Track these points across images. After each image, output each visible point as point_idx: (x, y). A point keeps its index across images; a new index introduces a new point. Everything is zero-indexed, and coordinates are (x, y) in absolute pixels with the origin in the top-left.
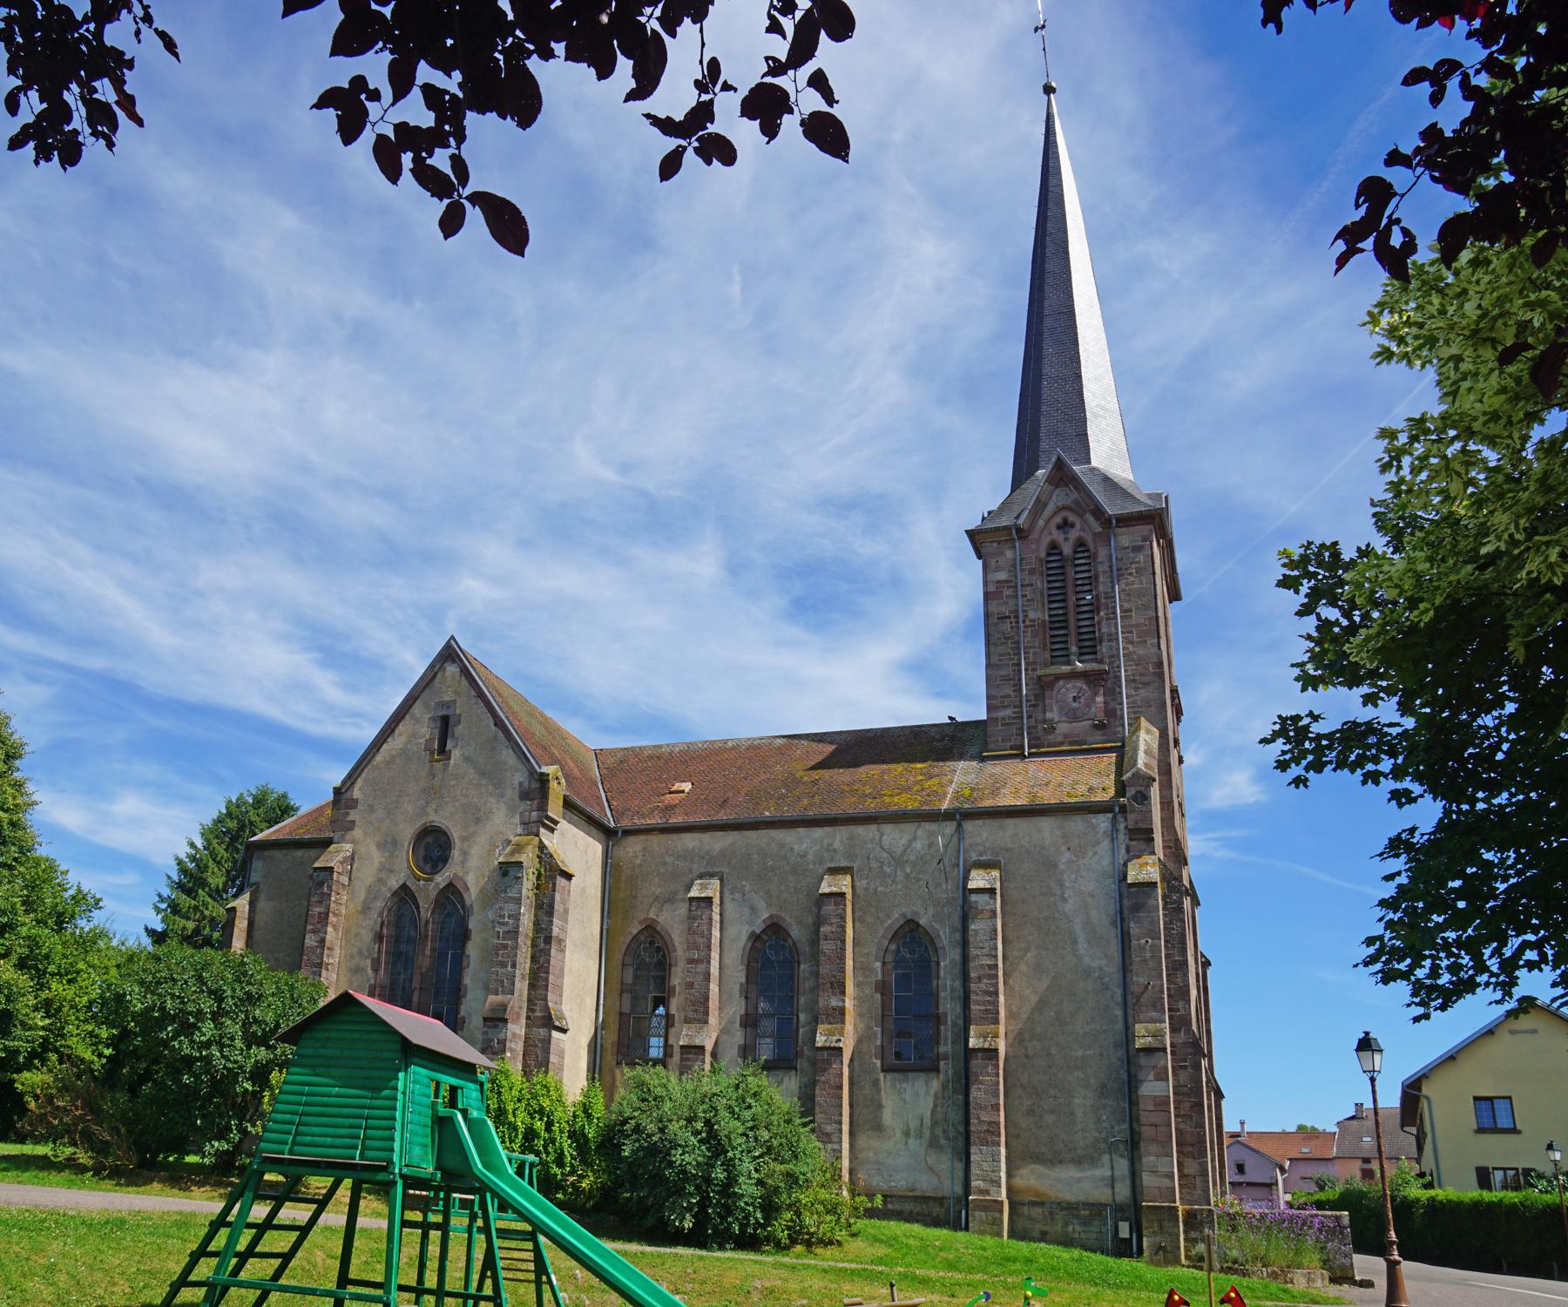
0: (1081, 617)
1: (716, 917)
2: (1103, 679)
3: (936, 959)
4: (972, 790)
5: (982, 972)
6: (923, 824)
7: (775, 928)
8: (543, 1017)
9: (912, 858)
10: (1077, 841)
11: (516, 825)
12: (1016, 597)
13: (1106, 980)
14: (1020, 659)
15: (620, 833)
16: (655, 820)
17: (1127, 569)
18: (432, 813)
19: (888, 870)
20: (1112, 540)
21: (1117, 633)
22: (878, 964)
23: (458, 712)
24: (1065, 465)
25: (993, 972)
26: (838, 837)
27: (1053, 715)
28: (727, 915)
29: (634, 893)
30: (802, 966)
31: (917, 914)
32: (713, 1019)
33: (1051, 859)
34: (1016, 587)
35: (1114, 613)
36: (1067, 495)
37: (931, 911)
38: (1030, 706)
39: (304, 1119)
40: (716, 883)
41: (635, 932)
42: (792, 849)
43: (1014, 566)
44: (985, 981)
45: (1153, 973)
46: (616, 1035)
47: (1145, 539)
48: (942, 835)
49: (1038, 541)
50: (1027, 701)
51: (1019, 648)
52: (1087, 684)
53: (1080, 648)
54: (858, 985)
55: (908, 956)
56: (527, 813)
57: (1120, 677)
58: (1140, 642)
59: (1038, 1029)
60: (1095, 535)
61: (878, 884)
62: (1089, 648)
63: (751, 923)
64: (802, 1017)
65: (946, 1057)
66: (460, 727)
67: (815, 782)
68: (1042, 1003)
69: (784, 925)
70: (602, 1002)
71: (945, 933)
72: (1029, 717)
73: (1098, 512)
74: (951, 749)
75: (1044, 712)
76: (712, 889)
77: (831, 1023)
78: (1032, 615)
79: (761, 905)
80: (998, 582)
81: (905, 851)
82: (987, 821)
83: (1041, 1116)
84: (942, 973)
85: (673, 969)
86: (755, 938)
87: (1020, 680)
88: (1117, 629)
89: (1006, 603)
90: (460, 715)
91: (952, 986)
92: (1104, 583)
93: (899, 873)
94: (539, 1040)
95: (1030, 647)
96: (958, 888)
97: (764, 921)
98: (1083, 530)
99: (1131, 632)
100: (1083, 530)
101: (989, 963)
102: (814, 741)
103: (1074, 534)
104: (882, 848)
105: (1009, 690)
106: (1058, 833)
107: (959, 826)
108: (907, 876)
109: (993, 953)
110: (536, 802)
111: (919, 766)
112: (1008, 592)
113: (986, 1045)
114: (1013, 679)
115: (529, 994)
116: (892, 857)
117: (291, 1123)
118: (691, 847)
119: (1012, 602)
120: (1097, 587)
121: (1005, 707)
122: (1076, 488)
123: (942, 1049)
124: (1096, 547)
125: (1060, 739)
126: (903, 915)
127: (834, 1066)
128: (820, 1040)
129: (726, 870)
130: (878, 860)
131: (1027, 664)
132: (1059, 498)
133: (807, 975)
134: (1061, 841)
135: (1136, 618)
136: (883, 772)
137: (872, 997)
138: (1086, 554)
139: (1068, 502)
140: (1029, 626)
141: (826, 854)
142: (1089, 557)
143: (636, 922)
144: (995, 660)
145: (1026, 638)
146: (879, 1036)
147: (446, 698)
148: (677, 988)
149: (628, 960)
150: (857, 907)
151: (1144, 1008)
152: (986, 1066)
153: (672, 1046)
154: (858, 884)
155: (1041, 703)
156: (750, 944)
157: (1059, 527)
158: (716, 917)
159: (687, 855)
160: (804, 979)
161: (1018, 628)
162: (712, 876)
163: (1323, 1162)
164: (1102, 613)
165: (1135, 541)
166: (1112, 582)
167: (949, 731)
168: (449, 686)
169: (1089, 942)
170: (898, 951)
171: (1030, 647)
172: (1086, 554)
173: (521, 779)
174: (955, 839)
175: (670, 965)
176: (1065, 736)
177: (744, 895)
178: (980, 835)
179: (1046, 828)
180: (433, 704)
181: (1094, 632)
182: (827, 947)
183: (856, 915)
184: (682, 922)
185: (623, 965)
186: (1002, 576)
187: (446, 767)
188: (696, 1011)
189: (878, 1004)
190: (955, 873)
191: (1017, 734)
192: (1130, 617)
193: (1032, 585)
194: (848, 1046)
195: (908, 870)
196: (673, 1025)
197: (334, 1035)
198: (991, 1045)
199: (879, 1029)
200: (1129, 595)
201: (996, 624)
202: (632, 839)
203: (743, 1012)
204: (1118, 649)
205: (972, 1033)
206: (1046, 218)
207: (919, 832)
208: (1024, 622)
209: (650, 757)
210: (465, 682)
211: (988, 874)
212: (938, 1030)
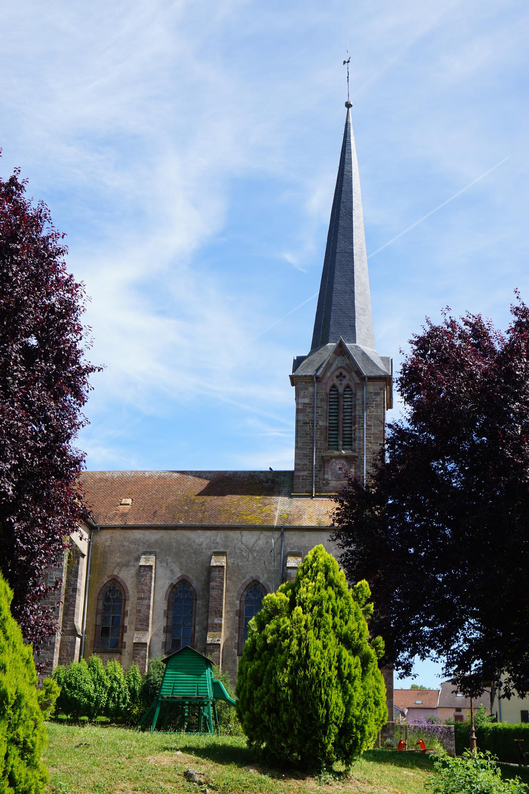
0: (345, 425)
1: (153, 575)
2: (355, 460)
4: (288, 515)
6: (263, 532)
7: (184, 582)
8: (72, 630)
9: (257, 549)
12: (314, 412)
14: (313, 446)
16: (118, 522)
17: (371, 404)
19: (245, 554)
20: (365, 388)
21: (363, 437)
22: (238, 602)
26: (219, 536)
27: (328, 476)
28: (158, 574)
29: (105, 561)
30: (198, 602)
31: (259, 577)
32: (150, 629)
34: (314, 407)
35: (363, 426)
36: (343, 360)
37: (266, 576)
38: (317, 471)
39: (199, 685)
40: (153, 558)
41: (105, 582)
42: (194, 541)
43: (313, 396)
46: (93, 637)
47: (381, 389)
48: (273, 539)
49: (326, 384)
50: (316, 468)
51: (313, 440)
52: (347, 462)
53: (343, 441)
54: (227, 612)
55: (253, 598)
57: (363, 460)
58: (374, 443)
60: (356, 384)
61: (239, 561)
62: (349, 442)
63: (171, 579)
64: (197, 628)
67: (203, 504)
70: (85, 619)
71: (272, 587)
72: (316, 476)
73: (359, 372)
74: (273, 488)
75: (324, 475)
76: (151, 561)
78: (321, 423)
80: (304, 404)
81: (254, 545)
82: (296, 532)
85: (127, 602)
86: (173, 587)
87: (313, 457)
88: (364, 435)
89: (307, 415)
92: (359, 410)
93: (250, 556)
94: (69, 642)
96: (280, 565)
97: (178, 578)
98: (350, 380)
99: (370, 437)
100: (350, 380)
102: (196, 476)
103: (345, 382)
104: (242, 543)
107: (282, 534)
108: (254, 558)
111: (258, 497)
114: (309, 456)
115: (63, 618)
117: (171, 686)
119: (311, 415)
120: (355, 411)
121: (304, 470)
122: (348, 358)
124: (356, 391)
125: (331, 489)
126: (252, 577)
128: (209, 640)
129: (158, 550)
131: (316, 449)
132: (338, 362)
135: (373, 430)
136: (239, 500)
138: (350, 393)
139: (343, 365)
141: (212, 545)
142: (352, 394)
143: (106, 577)
144: (300, 445)
145: (317, 435)
146: (237, 638)
148: (129, 612)
149: (101, 597)
150: (228, 572)
153: (125, 643)
154: (229, 561)
155: (322, 470)
156: (170, 590)
157: (337, 377)
158: (153, 575)
159: (136, 542)
161: (313, 429)
162: (150, 553)
163: (430, 710)
164: (357, 426)
165: (376, 390)
166: (363, 410)
167: (270, 476)
170: (247, 595)
171: (319, 440)
172: (350, 393)
174: (280, 540)
175: (125, 600)
176: (334, 488)
177: (167, 564)
178: (292, 539)
181: (352, 434)
182: (214, 593)
183: (228, 576)
184: (132, 577)
185: (98, 599)
186: (306, 401)
188: (142, 625)
189: (237, 622)
190: (279, 558)
191: (309, 485)
192: (371, 429)
193: (322, 407)
194: (222, 642)
195: (255, 555)
196: (126, 632)
197: (181, 659)
199: (237, 635)
200: (371, 418)
201: (301, 426)
202: (105, 532)
203: (165, 625)
204: (363, 445)
206: (341, 191)
207: (262, 536)
208: (316, 426)
209: (101, 480)
211: (296, 559)
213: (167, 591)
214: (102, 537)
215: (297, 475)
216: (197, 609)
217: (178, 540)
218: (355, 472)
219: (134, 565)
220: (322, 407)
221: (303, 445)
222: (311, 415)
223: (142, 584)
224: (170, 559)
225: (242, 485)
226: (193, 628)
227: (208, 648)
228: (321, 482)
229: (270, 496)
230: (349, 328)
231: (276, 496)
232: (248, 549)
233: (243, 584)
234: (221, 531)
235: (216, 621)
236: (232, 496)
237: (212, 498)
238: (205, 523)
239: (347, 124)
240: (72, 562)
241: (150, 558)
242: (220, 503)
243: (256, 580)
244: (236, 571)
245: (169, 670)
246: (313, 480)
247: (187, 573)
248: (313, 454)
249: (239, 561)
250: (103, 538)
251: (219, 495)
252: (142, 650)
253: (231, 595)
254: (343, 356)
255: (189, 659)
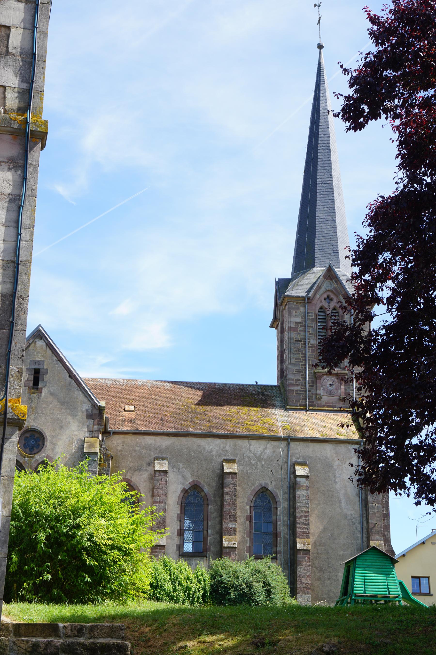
3: (275, 506)
5: (302, 514)
6: (270, 441)
9: (265, 457)
10: (342, 456)
11: (85, 432)
12: (305, 331)
13: (354, 520)
14: (306, 362)
15: (112, 433)
16: (129, 428)
18: (32, 421)
19: (253, 462)
22: (248, 507)
23: (45, 367)
24: (332, 270)
25: (307, 514)
26: (229, 444)
27: (320, 392)
29: (117, 465)
30: (210, 507)
31: (267, 484)
33: (330, 463)
34: (305, 326)
36: (331, 284)
37: (274, 483)
38: (309, 386)
40: (166, 463)
42: (204, 448)
43: (305, 316)
44: (303, 518)
45: (378, 519)
49: (315, 305)
50: (309, 383)
51: (305, 357)
56: (92, 426)
59: (323, 541)
61: (248, 468)
63: (183, 484)
64: (210, 531)
65: (280, 553)
66: (48, 376)
68: (325, 529)
69: (200, 486)
71: (280, 494)
72: (309, 391)
75: (317, 390)
77: (229, 535)
78: (312, 342)
79: (188, 475)
80: (296, 323)
81: (261, 453)
82: (301, 443)
83: (324, 581)
84: (279, 513)
86: (185, 491)
87: (306, 373)
89: (299, 334)
90: (47, 369)
91: (283, 520)
93: (258, 464)
95: (311, 357)
97: (190, 483)
101: (305, 510)
102: (187, 387)
104: (250, 451)
105: (300, 377)
106: (333, 451)
108: (262, 466)
109: (307, 505)
110: (96, 421)
112: (301, 329)
113: (305, 548)
114: (302, 372)
116: (255, 456)
118: (150, 443)
121: (298, 385)
122: (336, 282)
123: (278, 549)
126: (261, 485)
127: (232, 556)
129: (169, 456)
130: (248, 457)
131: (309, 365)
132: (327, 285)
133: (212, 511)
134: (335, 455)
137: (245, 523)
140: (310, 347)
141: (222, 452)
145: (309, 353)
146: (248, 542)
147: (37, 359)
151: (374, 534)
152: (305, 558)
156: (182, 494)
157: (325, 299)
159: (148, 447)
160: (211, 513)
162: (163, 459)
168: (39, 352)
169: (347, 503)
170: (256, 501)
171: (311, 357)
173: (87, 408)
176: (326, 403)
178: (298, 449)
179: (328, 449)
180: (29, 361)
184: (145, 481)
186: (298, 320)
187: (39, 397)
193: (312, 327)
197: (368, 558)
198: (307, 548)
199: (248, 538)
201: (294, 344)
202: (116, 436)
203: (178, 528)
205: (298, 542)
210: (49, 351)
211: (304, 468)
212: (277, 540)
213: (179, 496)
214: (114, 442)
215: (291, 390)
216: (209, 514)
217: (189, 447)
218: (345, 389)
219: (146, 470)
220: (312, 327)
221: (296, 362)
222: (302, 334)
223: (158, 488)
224: (181, 465)
225: (235, 396)
226: (205, 532)
227: (224, 551)
228: (314, 396)
229: (266, 408)
230: (333, 254)
231: (271, 408)
232: (256, 457)
233: (252, 490)
234: (230, 440)
235: (231, 525)
236: (230, 406)
237: (211, 407)
238: (215, 431)
239: (319, 64)
240: (102, 465)
241: (163, 463)
242: (221, 413)
243: (264, 487)
244: (246, 478)
245: (358, 569)
246: (306, 394)
247: (199, 478)
248: (306, 370)
249: (248, 468)
250: (115, 442)
251: (217, 406)
252: (160, 552)
253: (242, 501)
254: (331, 280)
255: (375, 559)
